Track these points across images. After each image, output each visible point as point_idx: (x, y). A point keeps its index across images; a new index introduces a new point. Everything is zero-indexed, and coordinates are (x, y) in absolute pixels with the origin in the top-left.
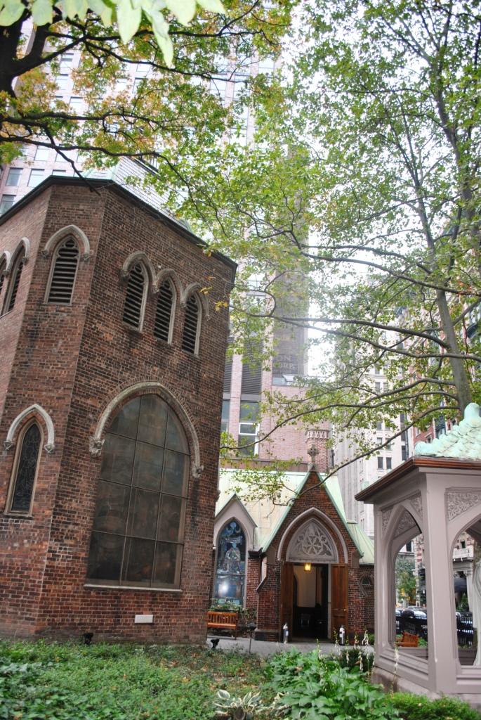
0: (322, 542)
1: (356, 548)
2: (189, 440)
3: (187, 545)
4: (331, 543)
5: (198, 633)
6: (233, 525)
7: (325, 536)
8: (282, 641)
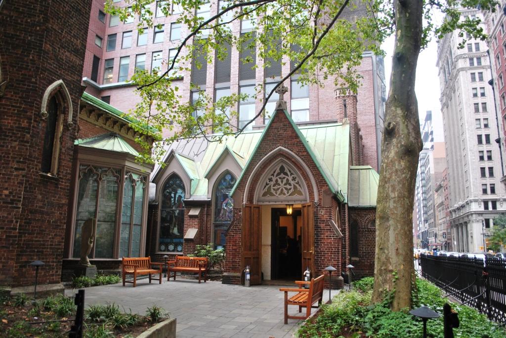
0: (274, 179)
1: (328, 186)
4: (302, 182)
6: (228, 178)
7: (295, 176)
8: (243, 284)
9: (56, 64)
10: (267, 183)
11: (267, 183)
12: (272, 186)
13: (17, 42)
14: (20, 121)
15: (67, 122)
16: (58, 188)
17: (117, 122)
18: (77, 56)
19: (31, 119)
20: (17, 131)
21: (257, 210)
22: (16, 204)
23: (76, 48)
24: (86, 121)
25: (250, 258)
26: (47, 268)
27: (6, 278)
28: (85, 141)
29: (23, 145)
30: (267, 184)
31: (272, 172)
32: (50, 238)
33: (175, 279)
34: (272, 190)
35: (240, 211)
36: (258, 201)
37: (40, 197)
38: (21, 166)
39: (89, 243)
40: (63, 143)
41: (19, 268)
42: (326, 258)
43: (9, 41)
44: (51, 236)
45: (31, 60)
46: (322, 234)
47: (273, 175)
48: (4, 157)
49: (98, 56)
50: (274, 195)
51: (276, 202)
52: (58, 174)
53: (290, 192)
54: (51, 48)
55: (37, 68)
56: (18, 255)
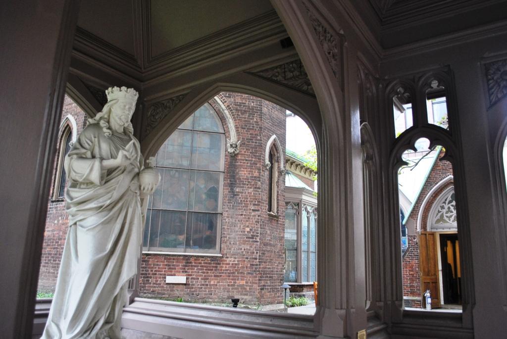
0: (446, 207)
2: (223, 119)
3: (225, 214)
5: (247, 295)
10: (439, 211)
11: (439, 211)
13: (244, 109)
14: (252, 172)
15: (280, 169)
17: (289, 160)
19: (260, 170)
20: (251, 179)
21: (432, 236)
22: (256, 239)
25: (429, 283)
26: (276, 290)
27: (252, 298)
29: (256, 191)
30: (439, 212)
31: (444, 200)
34: (445, 216)
35: (414, 238)
36: (431, 229)
38: (256, 208)
40: (279, 186)
43: (239, 109)
45: (255, 122)
47: (445, 203)
48: (244, 201)
50: (447, 222)
51: (450, 228)
52: (278, 213)
55: (260, 128)
56: (259, 280)
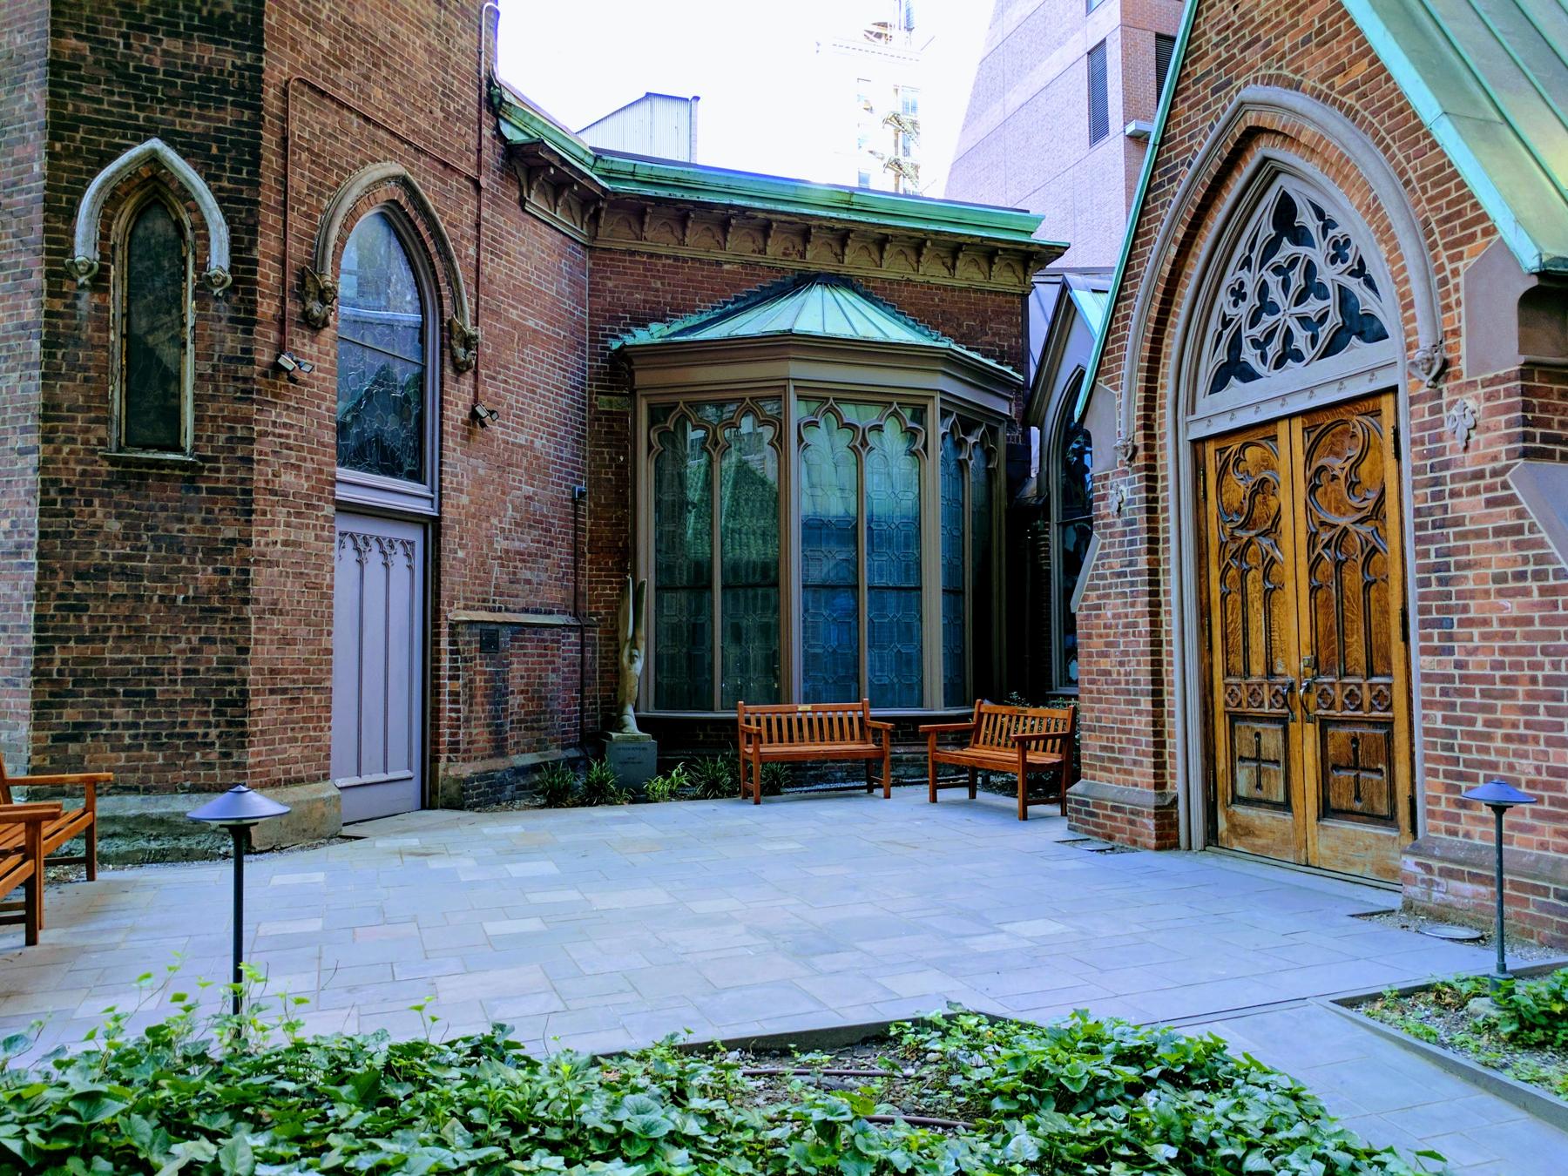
7: (1224, 298)
9: (121, 94)
12: (1245, 322)
16: (198, 490)
18: (217, 42)
23: (211, 13)
24: (676, 259)
28: (676, 327)
32: (183, 651)
33: (973, 795)
37: (115, 526)
39: (625, 660)
41: (49, 742)
42: (1498, 724)
44: (183, 645)
46: (1468, 565)
49: (1165, 32)
53: (1324, 333)
54: (85, 47)
